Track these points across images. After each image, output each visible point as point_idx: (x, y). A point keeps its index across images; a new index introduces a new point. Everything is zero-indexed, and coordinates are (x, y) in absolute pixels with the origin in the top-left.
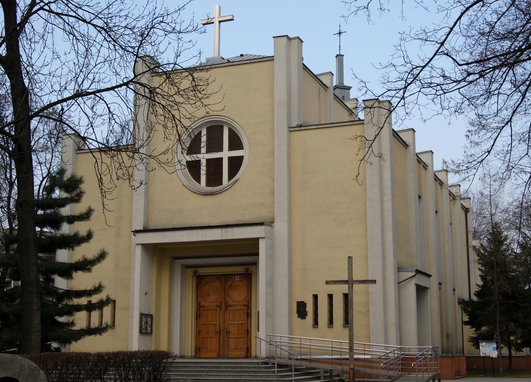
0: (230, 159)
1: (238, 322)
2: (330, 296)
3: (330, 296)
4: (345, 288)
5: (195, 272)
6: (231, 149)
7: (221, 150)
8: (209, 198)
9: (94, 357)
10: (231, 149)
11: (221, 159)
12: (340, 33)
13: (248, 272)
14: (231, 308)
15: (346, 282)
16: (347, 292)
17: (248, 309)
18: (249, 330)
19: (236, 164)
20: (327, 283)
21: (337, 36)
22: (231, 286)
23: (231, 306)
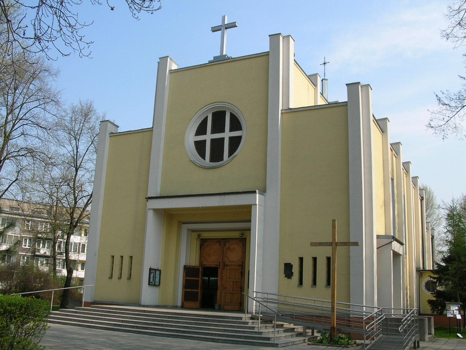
0: (231, 139)
1: (233, 280)
2: (315, 259)
3: (315, 259)
4: (327, 251)
5: (199, 236)
6: (231, 130)
7: (223, 131)
8: (211, 171)
9: (244, 328)
10: (231, 130)
11: (223, 139)
12: (325, 64)
13: (243, 237)
14: (228, 267)
15: (330, 244)
16: (330, 255)
17: (242, 268)
18: (288, 328)
19: (235, 142)
20: (313, 244)
21: (323, 66)
22: (229, 248)
23: (227, 265)
